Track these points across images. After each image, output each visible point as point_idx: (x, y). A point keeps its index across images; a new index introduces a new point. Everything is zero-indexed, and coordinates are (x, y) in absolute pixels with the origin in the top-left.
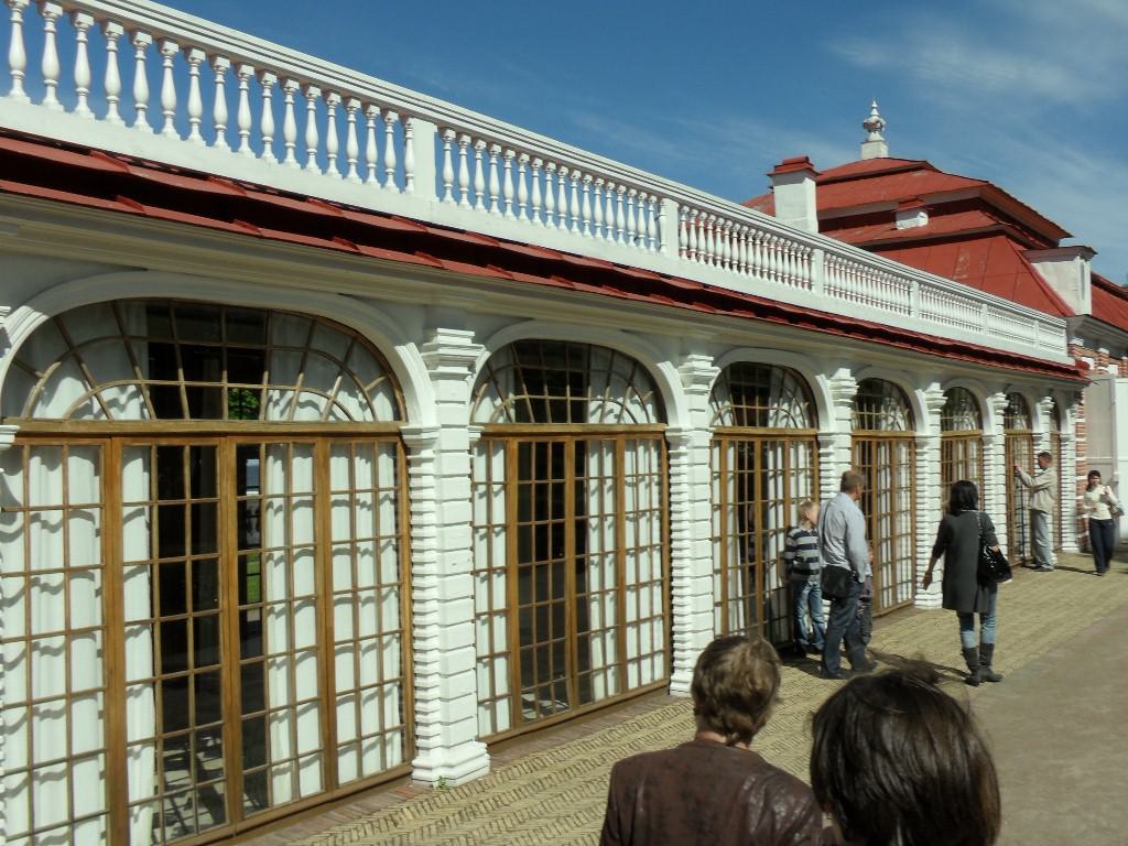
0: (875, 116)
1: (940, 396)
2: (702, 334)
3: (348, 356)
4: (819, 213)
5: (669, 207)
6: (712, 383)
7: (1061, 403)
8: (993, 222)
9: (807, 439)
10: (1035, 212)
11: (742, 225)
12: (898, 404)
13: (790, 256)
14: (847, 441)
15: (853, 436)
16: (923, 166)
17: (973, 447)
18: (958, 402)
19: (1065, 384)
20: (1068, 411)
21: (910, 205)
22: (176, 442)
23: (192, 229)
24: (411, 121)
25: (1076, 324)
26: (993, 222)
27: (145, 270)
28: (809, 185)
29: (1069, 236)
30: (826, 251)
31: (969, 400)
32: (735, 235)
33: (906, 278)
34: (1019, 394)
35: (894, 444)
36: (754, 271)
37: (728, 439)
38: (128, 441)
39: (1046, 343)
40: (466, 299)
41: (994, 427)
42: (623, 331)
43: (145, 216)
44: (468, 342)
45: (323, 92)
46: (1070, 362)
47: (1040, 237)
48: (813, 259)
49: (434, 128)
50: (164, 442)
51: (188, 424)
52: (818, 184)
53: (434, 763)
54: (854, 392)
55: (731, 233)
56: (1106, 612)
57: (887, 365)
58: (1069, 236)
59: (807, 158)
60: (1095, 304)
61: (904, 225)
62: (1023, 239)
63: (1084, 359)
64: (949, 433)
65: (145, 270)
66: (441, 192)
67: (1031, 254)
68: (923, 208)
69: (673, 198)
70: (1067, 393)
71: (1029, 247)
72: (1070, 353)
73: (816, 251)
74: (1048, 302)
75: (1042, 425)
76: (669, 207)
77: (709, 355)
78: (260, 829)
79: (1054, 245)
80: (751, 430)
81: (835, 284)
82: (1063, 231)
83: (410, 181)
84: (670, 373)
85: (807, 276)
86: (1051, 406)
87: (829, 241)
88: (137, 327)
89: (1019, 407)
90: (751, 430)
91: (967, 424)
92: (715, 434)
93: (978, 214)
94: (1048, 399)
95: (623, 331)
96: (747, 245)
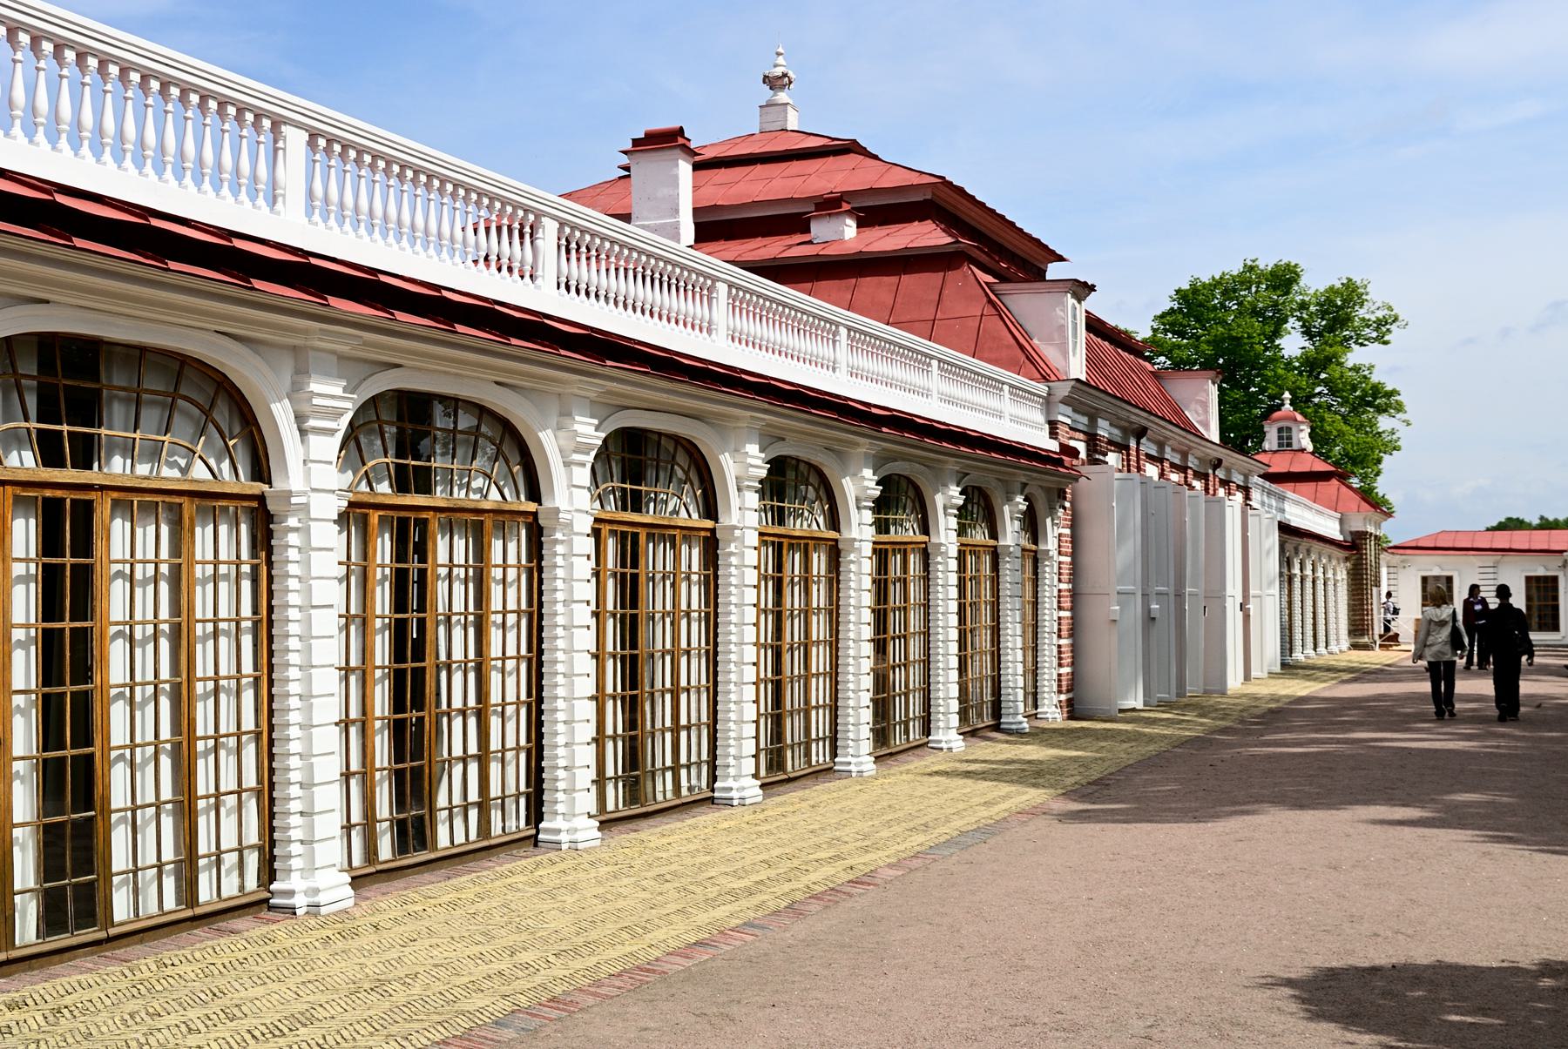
0: (780, 50)
1: (873, 484)
2: (577, 385)
3: (212, 405)
4: (696, 211)
5: (295, 140)
6: (593, 453)
7: (1041, 507)
8: (950, 240)
9: (703, 534)
10: (1012, 224)
11: (630, 250)
12: (818, 498)
13: (644, 278)
14: (753, 539)
15: (761, 534)
16: (851, 148)
17: (914, 561)
18: (899, 497)
19: (1043, 477)
20: (1049, 521)
21: (829, 205)
22: (59, 493)
23: (99, 259)
24: (283, 128)
25: (1063, 390)
26: (950, 240)
27: (47, 302)
28: (685, 168)
29: (1061, 259)
30: (731, 285)
31: (911, 493)
32: (573, 245)
33: (831, 322)
34: (979, 489)
35: (811, 548)
36: (578, 291)
37: (608, 527)
38: (18, 491)
39: (1021, 423)
40: (345, 342)
41: (946, 533)
42: (498, 383)
43: (74, 248)
44: (339, 391)
45: (142, 77)
46: (1054, 446)
47: (1015, 257)
48: (540, 235)
49: (306, 136)
50: (48, 493)
51: (69, 475)
52: (697, 167)
53: (294, 884)
54: (763, 473)
55: (579, 247)
56: (1084, 782)
57: (805, 439)
58: (1061, 259)
59: (681, 131)
60: (1092, 361)
61: (821, 230)
62: (992, 264)
63: (1072, 443)
64: (884, 538)
65: (47, 302)
66: (310, 211)
67: (1003, 287)
68: (850, 213)
69: (725, 281)
70: (1048, 490)
71: (1003, 278)
72: (1053, 434)
73: (719, 284)
74: (1027, 359)
75: (1011, 535)
76: (295, 140)
77: (592, 417)
78: (124, 941)
79: (1040, 275)
80: (636, 517)
81: (728, 323)
82: (1053, 252)
83: (280, 199)
84: (549, 443)
85: (707, 317)
86: (1023, 507)
87: (710, 261)
88: (28, 367)
89: (979, 508)
90: (636, 517)
91: (908, 532)
92: (597, 520)
93: (929, 225)
94: (1019, 499)
95: (498, 383)
96: (578, 259)
